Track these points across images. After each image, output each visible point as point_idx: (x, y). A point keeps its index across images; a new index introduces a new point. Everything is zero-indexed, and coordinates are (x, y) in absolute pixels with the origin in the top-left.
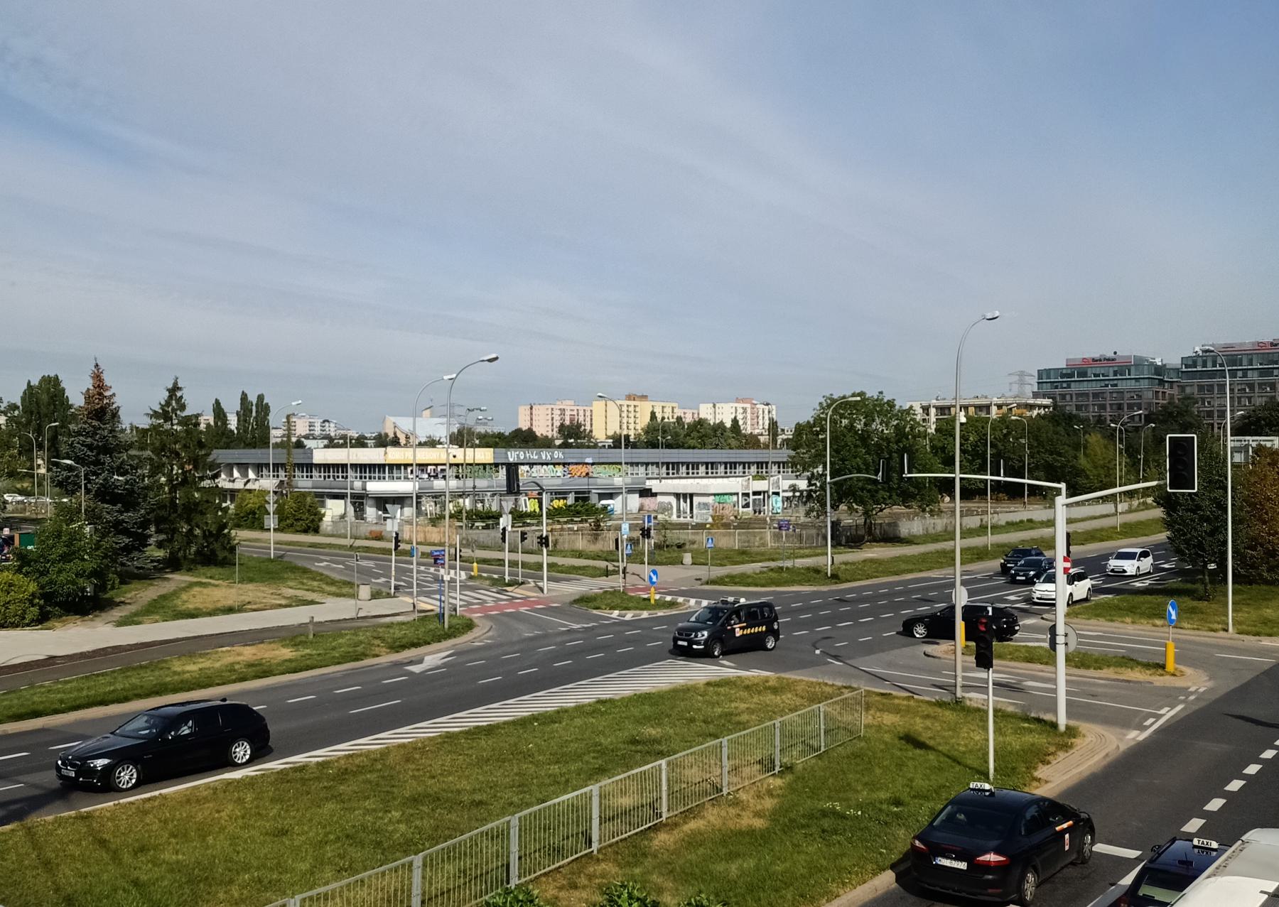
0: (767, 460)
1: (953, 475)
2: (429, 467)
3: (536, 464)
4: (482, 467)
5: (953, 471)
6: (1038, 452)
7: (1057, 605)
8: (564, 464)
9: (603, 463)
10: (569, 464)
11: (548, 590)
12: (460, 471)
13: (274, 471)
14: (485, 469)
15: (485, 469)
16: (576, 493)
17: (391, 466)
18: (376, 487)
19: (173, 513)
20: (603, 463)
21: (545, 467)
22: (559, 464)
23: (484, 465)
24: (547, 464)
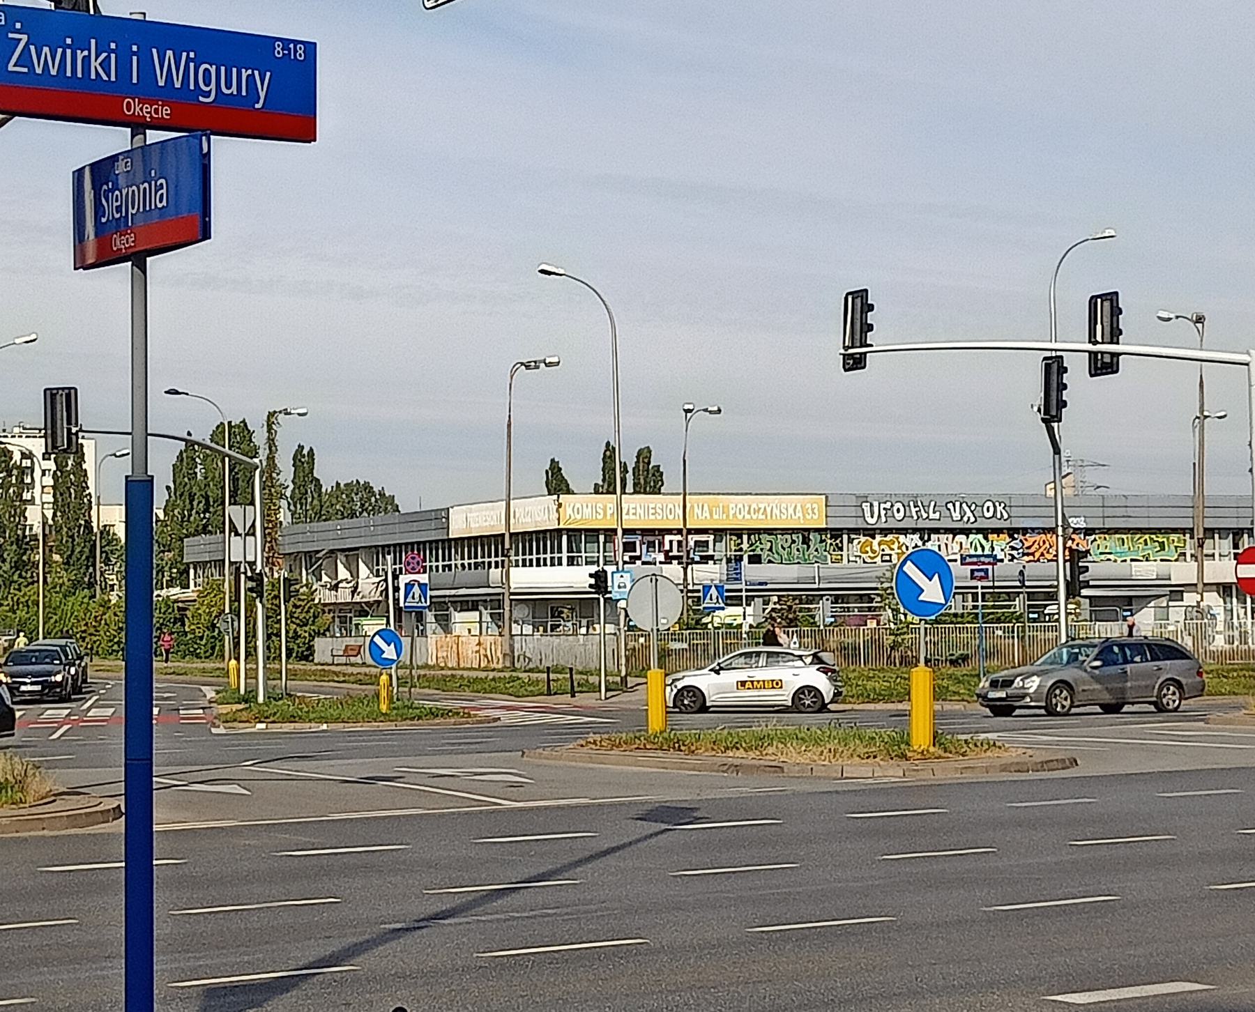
0: (49, 468)
1: (983, 611)
2: (668, 538)
3: (936, 531)
4: (798, 538)
5: (742, 596)
6: (974, 900)
7: (914, 714)
8: (1012, 532)
9: (1117, 531)
10: (1025, 531)
11: (268, 697)
12: (745, 546)
13: (570, 550)
14: (806, 541)
15: (806, 541)
16: (837, 599)
17: (573, 534)
18: (526, 578)
19: (693, 601)
20: (1117, 531)
21: (961, 538)
22: (998, 531)
23: (805, 533)
24: (966, 532)
